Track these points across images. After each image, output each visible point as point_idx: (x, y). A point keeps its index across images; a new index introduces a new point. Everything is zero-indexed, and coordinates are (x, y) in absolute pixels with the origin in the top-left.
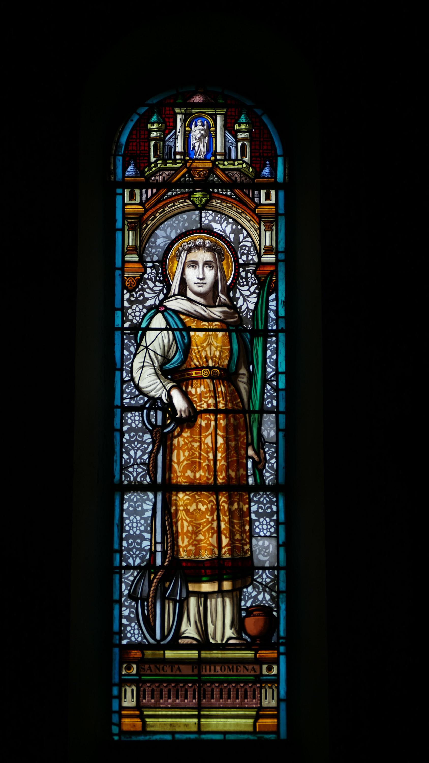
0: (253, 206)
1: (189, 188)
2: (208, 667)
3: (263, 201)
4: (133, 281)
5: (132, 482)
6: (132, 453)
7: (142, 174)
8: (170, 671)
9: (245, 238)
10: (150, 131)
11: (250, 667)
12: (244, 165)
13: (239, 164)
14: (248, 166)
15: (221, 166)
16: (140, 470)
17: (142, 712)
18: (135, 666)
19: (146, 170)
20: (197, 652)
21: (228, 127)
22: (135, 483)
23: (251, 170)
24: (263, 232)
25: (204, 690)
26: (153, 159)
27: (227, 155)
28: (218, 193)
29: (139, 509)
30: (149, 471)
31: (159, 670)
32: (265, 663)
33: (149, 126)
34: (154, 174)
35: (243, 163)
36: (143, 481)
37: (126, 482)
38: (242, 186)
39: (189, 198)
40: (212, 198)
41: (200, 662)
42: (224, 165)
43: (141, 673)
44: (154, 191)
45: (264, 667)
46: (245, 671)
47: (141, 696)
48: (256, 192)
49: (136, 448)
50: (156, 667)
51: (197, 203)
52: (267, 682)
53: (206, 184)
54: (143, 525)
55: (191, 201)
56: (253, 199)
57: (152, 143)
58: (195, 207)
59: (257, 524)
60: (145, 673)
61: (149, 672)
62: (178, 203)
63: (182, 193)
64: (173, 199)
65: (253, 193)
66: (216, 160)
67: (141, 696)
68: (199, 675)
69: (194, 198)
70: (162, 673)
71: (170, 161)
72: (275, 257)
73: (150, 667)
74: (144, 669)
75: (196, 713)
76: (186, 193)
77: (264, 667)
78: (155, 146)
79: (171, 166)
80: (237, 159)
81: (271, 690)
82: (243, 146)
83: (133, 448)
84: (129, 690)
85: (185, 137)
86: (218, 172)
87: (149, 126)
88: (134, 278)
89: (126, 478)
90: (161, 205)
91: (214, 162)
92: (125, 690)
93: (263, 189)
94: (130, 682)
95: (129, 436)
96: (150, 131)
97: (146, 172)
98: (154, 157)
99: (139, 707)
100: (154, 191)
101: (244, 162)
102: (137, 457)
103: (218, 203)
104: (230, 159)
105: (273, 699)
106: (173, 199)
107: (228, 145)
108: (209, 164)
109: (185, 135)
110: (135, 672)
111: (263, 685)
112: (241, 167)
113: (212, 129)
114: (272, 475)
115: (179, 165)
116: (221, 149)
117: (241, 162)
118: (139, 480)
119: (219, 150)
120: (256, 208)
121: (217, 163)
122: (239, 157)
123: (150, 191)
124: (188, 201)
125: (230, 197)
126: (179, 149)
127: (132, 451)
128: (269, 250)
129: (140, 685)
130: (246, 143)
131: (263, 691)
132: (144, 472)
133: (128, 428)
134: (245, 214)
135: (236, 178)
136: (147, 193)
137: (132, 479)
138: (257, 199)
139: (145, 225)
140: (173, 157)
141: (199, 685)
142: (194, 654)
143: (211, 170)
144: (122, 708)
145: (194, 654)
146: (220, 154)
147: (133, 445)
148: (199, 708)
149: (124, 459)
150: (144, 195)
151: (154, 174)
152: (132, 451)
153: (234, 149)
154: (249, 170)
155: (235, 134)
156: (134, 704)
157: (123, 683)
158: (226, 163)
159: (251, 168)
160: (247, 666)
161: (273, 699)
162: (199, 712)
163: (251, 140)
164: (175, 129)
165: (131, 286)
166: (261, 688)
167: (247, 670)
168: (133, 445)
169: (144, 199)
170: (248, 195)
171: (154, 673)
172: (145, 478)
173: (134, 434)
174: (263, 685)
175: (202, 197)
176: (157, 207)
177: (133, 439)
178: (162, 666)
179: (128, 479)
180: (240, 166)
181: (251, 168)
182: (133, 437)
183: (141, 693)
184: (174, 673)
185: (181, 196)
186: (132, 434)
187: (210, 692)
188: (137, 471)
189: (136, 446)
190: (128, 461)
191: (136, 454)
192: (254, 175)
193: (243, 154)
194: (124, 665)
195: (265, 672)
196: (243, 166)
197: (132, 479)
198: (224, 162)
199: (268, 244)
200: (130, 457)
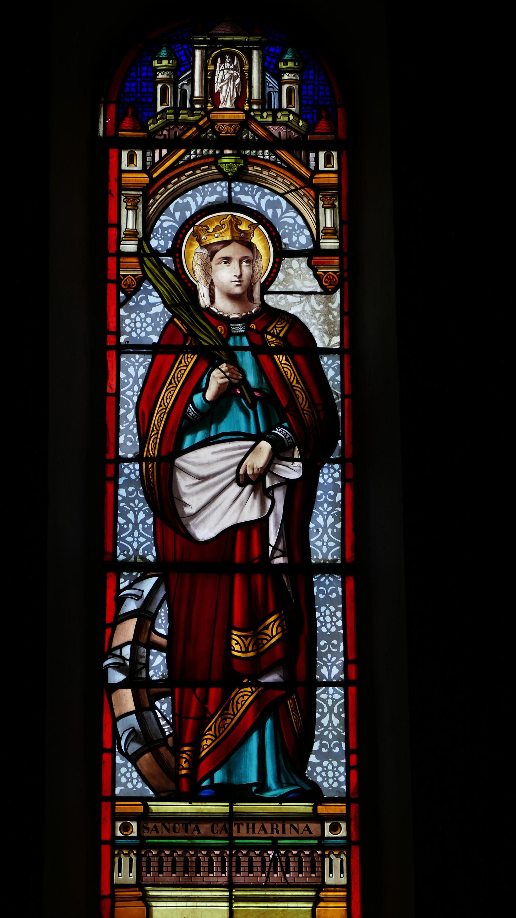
0: (307, 174)
1: (215, 148)
2: (280, 826)
3: (322, 167)
4: (333, 277)
5: (131, 557)
6: (131, 516)
7: (144, 128)
8: (245, 831)
9: (283, 213)
10: (156, 70)
11: (302, 826)
12: (291, 117)
13: (282, 115)
14: (297, 119)
15: (258, 118)
16: (129, 539)
17: (145, 892)
18: (134, 825)
19: (151, 121)
20: (227, 804)
21: (270, 68)
22: (136, 558)
23: (301, 123)
24: (321, 210)
25: (238, 861)
26: (159, 108)
27: (265, 101)
28: (256, 157)
29: (144, 303)
30: (155, 540)
31: (168, 830)
32: (328, 820)
33: (155, 63)
34: (162, 128)
35: (289, 115)
36: (148, 555)
37: (121, 558)
38: (289, 145)
39: (215, 163)
40: (247, 163)
41: (231, 818)
42: (262, 117)
43: (145, 835)
44: (164, 152)
45: (327, 825)
46: (293, 831)
47: (144, 869)
48: (312, 155)
49: (136, 509)
50: (292, 826)
51: (226, 170)
52: (332, 848)
53: (237, 147)
54: (150, 324)
55: (218, 168)
56: (306, 165)
57: (159, 86)
58: (223, 175)
59: (127, 321)
60: (149, 835)
61: (154, 834)
62: (199, 171)
63: (203, 157)
64: (193, 164)
65: (308, 156)
66: (251, 110)
67: (144, 869)
68: (231, 838)
69: (222, 163)
70: (172, 834)
71: (185, 112)
72: (338, 241)
73: (263, 826)
74: (148, 829)
75: (227, 894)
76: (208, 156)
77: (327, 825)
78: (164, 91)
79: (187, 117)
80: (280, 109)
81: (339, 859)
82: (290, 91)
83: (132, 509)
84: (336, 862)
85: (206, 78)
86: (254, 126)
87: (155, 63)
88: (134, 276)
89: (122, 551)
90: (176, 171)
91: (247, 113)
92: (331, 860)
93: (322, 150)
94: (130, 848)
95: (127, 491)
96: (156, 70)
97: (150, 125)
98: (161, 105)
99: (140, 885)
100: (164, 152)
101: (291, 112)
102: (138, 522)
103: (257, 171)
104: (270, 109)
105: (342, 872)
106: (193, 164)
107: (268, 90)
108: (241, 116)
109: (206, 75)
110: (135, 834)
111: (327, 853)
112: (287, 120)
113: (246, 67)
114: (123, 539)
115: (197, 117)
116: (202, 92)
117: (287, 113)
118: (141, 553)
119: (256, 95)
120: (312, 177)
121: (252, 114)
122: (285, 105)
123: (157, 152)
124: (213, 168)
125: (274, 163)
126: (256, 95)
127: (131, 512)
128: (329, 233)
129: (116, 853)
130: (168, 86)
131: (327, 860)
132: (149, 543)
133: (124, 481)
134: (281, 177)
135: (280, 133)
136: (153, 157)
137: (131, 552)
138: (312, 164)
139: (152, 201)
140: (188, 106)
141: (231, 852)
142: (220, 808)
143: (244, 125)
144: (115, 887)
145: (220, 808)
146: (198, 102)
147: (132, 504)
148: (231, 885)
149: (120, 524)
150: (149, 159)
151: (162, 128)
152: (131, 512)
153: (277, 95)
154: (298, 124)
155: (278, 75)
156: (132, 879)
157: (117, 847)
158: (265, 114)
159: (301, 121)
160: (296, 825)
161: (131, 871)
162: (231, 892)
163: (301, 83)
164: (193, 68)
165: (129, 288)
166: (323, 856)
167: (297, 830)
168: (132, 504)
169: (149, 163)
170: (299, 160)
171: (160, 835)
172: (150, 552)
173: (134, 489)
174: (327, 853)
175: (233, 163)
176: (171, 174)
177: (133, 496)
178: (172, 825)
179: (126, 552)
180: (286, 119)
181: (301, 121)
182: (132, 493)
183: (144, 864)
184: (189, 834)
185: (203, 161)
186: (130, 489)
187: (194, 864)
188: (138, 541)
189: (136, 506)
190: (125, 526)
191: (136, 517)
192: (305, 130)
193: (289, 102)
194: (118, 824)
195: (327, 833)
196: (289, 118)
197: (131, 552)
198: (262, 113)
199: (130, 226)
200: (128, 521)
